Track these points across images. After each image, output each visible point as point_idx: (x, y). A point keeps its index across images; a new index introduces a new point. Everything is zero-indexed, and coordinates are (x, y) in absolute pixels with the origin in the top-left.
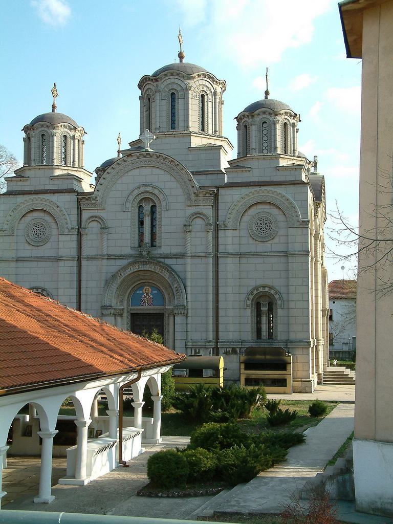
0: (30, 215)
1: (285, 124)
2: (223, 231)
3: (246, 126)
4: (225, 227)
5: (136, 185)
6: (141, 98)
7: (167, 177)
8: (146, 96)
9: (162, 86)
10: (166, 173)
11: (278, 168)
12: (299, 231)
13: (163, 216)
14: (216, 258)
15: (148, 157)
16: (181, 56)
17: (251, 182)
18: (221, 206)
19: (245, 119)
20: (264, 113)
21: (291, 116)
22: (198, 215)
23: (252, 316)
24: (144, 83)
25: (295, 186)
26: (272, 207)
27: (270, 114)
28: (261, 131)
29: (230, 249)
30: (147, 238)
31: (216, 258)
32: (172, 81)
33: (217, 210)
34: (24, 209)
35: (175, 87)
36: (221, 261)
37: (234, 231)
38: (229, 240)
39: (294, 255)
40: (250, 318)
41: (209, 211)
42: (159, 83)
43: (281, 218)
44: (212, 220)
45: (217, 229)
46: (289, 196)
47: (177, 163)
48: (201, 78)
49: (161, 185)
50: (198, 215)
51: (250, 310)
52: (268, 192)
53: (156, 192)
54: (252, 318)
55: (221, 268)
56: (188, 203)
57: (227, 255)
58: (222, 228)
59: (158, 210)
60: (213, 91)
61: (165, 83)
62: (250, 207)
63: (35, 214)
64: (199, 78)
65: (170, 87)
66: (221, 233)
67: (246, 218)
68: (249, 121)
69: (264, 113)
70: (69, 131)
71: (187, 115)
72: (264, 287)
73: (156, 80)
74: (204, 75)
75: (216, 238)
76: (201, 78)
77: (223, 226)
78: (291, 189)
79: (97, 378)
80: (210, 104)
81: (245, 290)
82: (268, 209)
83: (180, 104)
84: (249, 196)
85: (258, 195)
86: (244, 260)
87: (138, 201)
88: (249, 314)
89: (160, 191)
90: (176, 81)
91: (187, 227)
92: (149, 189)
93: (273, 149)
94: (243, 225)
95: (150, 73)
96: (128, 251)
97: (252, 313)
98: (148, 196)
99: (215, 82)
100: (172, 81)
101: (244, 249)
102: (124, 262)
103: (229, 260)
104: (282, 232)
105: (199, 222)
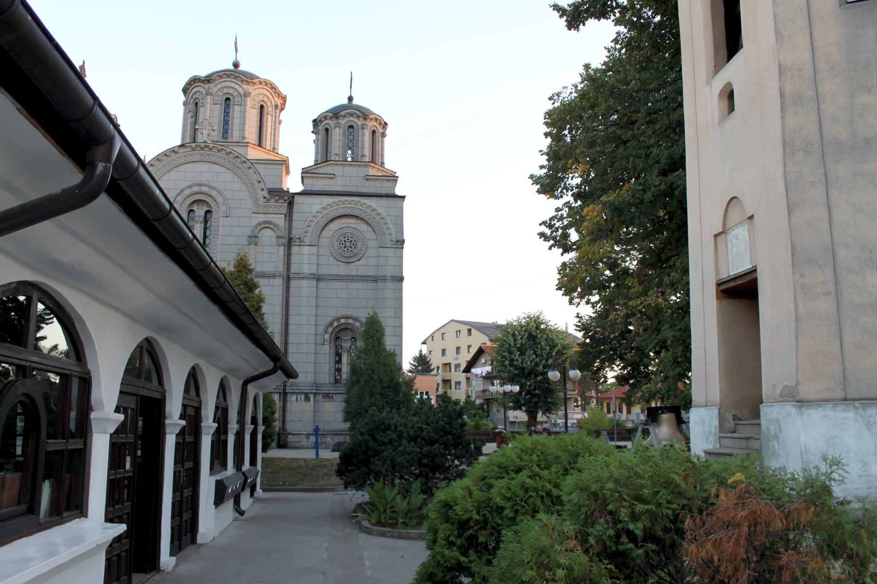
1: (374, 132)
4: (301, 242)
7: (230, 176)
8: (192, 101)
9: (216, 89)
10: (228, 171)
11: (367, 177)
12: (391, 252)
13: (221, 224)
14: (288, 279)
15: (206, 151)
18: (295, 217)
19: (326, 122)
20: (352, 115)
21: (380, 124)
23: (330, 354)
24: (192, 86)
25: (389, 199)
26: (359, 222)
27: (358, 117)
29: (307, 269)
31: (288, 279)
32: (229, 84)
33: (290, 220)
35: (231, 91)
36: (293, 283)
37: (312, 247)
38: (306, 259)
39: (384, 279)
40: (328, 356)
41: (280, 220)
42: (211, 85)
43: (370, 235)
44: (283, 233)
45: (289, 243)
46: (381, 210)
48: (262, 87)
49: (220, 187)
51: (328, 346)
52: (356, 204)
54: (330, 356)
55: (293, 291)
56: (255, 210)
58: (297, 244)
61: (219, 86)
62: (332, 220)
64: (261, 86)
65: (225, 91)
66: (295, 249)
67: (327, 233)
68: (332, 123)
69: (352, 115)
71: (243, 124)
72: (346, 318)
73: (209, 82)
75: (288, 255)
76: (262, 87)
77: (298, 240)
78: (384, 201)
79: (110, 497)
80: (270, 117)
81: (324, 322)
82: (354, 224)
83: (236, 111)
84: (327, 209)
85: (331, 209)
86: (322, 284)
87: (188, 203)
88: (327, 350)
89: (218, 193)
90: (233, 85)
94: (323, 242)
95: (203, 73)
97: (330, 349)
98: (205, 199)
99: (276, 95)
100: (229, 84)
101: (324, 271)
103: (305, 283)
104: (371, 252)
105: (268, 233)
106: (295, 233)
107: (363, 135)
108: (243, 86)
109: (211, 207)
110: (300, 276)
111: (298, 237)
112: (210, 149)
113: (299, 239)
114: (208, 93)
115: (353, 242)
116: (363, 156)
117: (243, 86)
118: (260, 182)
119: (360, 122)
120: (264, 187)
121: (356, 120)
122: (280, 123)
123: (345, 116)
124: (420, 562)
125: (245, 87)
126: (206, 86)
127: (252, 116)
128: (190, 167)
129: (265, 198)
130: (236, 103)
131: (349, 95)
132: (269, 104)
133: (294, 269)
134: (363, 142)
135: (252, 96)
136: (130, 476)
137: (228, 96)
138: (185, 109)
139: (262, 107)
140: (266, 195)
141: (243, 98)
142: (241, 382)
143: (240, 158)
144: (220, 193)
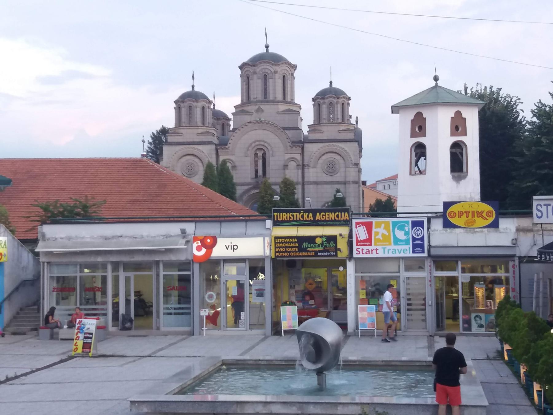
0: (184, 158)
1: (343, 104)
2: (307, 169)
3: (319, 104)
5: (253, 140)
6: (241, 76)
8: (245, 75)
14: (303, 185)
15: (261, 124)
16: (267, 47)
17: (323, 140)
18: (306, 154)
21: (346, 99)
22: (293, 159)
26: (336, 154)
27: (334, 98)
28: (329, 108)
29: (312, 180)
30: (260, 173)
31: (303, 185)
34: (180, 154)
35: (267, 71)
36: (306, 186)
41: (298, 157)
44: (301, 163)
45: (303, 166)
46: (346, 149)
47: (272, 123)
49: (268, 141)
50: (293, 159)
53: (266, 145)
57: (310, 183)
59: (267, 155)
60: (290, 72)
61: (260, 68)
62: (323, 155)
63: (333, 155)
64: (283, 65)
65: (264, 71)
66: (306, 170)
67: (321, 161)
68: (322, 101)
70: (205, 104)
71: (275, 90)
74: (286, 63)
80: (289, 81)
83: (270, 82)
91: (285, 167)
92: (262, 143)
93: (336, 120)
94: (319, 165)
96: (249, 180)
101: (320, 180)
102: (246, 188)
104: (342, 170)
106: (306, 162)
107: (337, 107)
108: (273, 67)
109: (265, 151)
110: (309, 183)
111: (307, 164)
112: (263, 123)
113: (308, 165)
114: (255, 73)
115: (334, 165)
116: (338, 119)
117: (273, 67)
118: (287, 138)
119: (335, 100)
120: (290, 141)
121: (333, 99)
122: (294, 79)
123: (327, 98)
124: (234, 178)
125: (274, 67)
126: (253, 68)
127: (280, 82)
128: (253, 132)
129: (290, 146)
130: (270, 78)
131: (330, 81)
132: (288, 74)
133: (306, 180)
134: (337, 111)
135: (278, 72)
136: (338, 193)
137: (266, 74)
138: (241, 79)
139: (284, 76)
140: (291, 145)
141: (274, 74)
142: (543, 217)
143: (277, 127)
144: (268, 144)
